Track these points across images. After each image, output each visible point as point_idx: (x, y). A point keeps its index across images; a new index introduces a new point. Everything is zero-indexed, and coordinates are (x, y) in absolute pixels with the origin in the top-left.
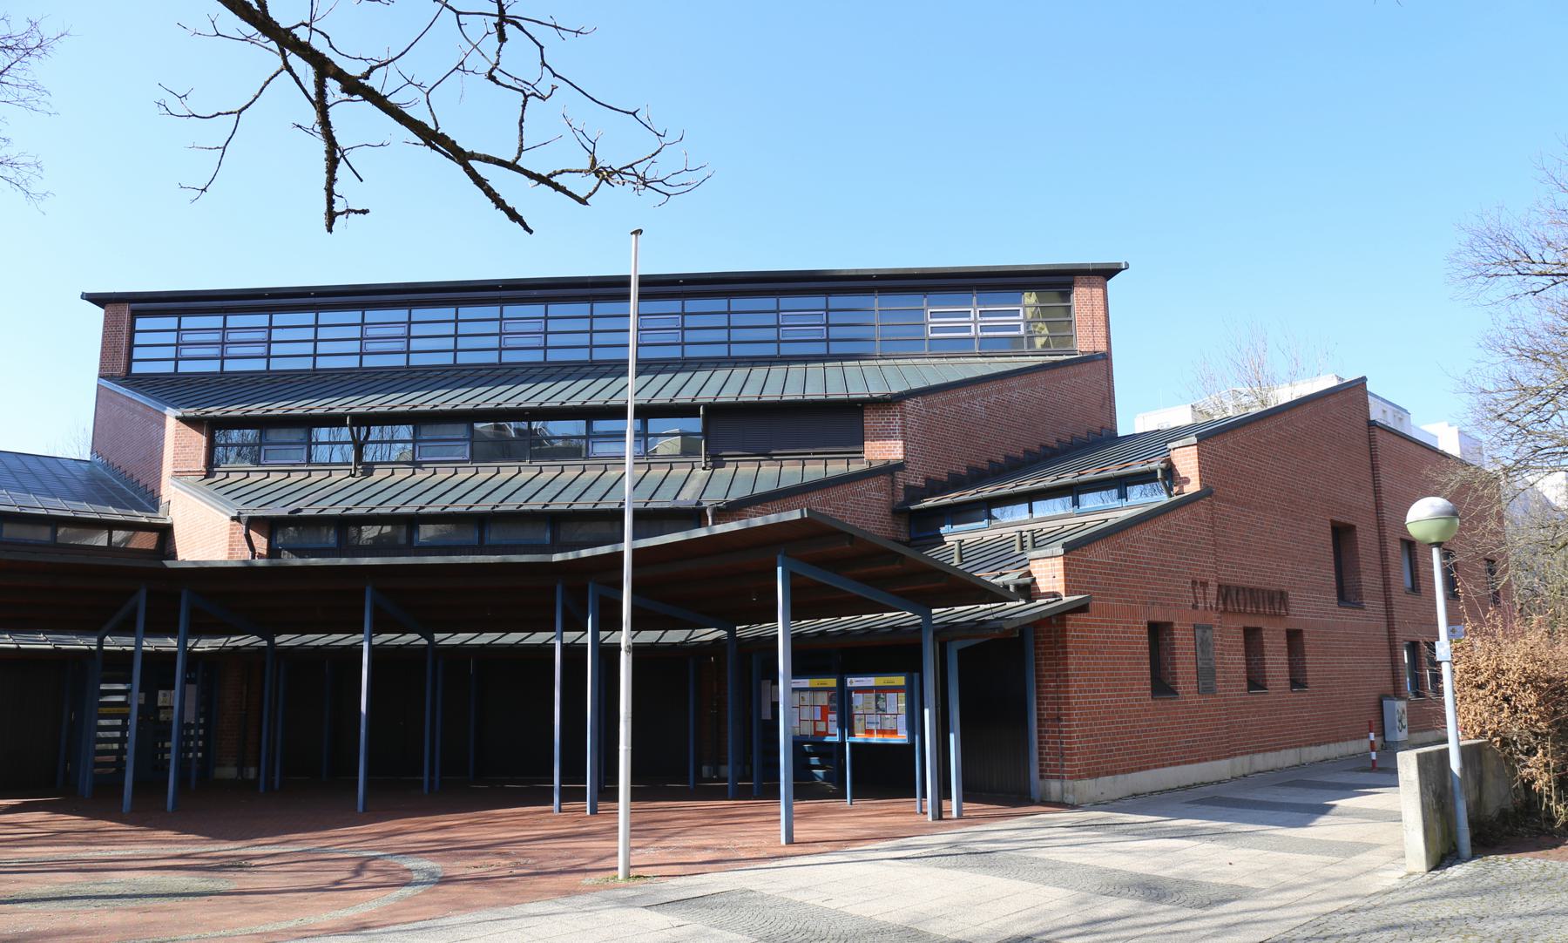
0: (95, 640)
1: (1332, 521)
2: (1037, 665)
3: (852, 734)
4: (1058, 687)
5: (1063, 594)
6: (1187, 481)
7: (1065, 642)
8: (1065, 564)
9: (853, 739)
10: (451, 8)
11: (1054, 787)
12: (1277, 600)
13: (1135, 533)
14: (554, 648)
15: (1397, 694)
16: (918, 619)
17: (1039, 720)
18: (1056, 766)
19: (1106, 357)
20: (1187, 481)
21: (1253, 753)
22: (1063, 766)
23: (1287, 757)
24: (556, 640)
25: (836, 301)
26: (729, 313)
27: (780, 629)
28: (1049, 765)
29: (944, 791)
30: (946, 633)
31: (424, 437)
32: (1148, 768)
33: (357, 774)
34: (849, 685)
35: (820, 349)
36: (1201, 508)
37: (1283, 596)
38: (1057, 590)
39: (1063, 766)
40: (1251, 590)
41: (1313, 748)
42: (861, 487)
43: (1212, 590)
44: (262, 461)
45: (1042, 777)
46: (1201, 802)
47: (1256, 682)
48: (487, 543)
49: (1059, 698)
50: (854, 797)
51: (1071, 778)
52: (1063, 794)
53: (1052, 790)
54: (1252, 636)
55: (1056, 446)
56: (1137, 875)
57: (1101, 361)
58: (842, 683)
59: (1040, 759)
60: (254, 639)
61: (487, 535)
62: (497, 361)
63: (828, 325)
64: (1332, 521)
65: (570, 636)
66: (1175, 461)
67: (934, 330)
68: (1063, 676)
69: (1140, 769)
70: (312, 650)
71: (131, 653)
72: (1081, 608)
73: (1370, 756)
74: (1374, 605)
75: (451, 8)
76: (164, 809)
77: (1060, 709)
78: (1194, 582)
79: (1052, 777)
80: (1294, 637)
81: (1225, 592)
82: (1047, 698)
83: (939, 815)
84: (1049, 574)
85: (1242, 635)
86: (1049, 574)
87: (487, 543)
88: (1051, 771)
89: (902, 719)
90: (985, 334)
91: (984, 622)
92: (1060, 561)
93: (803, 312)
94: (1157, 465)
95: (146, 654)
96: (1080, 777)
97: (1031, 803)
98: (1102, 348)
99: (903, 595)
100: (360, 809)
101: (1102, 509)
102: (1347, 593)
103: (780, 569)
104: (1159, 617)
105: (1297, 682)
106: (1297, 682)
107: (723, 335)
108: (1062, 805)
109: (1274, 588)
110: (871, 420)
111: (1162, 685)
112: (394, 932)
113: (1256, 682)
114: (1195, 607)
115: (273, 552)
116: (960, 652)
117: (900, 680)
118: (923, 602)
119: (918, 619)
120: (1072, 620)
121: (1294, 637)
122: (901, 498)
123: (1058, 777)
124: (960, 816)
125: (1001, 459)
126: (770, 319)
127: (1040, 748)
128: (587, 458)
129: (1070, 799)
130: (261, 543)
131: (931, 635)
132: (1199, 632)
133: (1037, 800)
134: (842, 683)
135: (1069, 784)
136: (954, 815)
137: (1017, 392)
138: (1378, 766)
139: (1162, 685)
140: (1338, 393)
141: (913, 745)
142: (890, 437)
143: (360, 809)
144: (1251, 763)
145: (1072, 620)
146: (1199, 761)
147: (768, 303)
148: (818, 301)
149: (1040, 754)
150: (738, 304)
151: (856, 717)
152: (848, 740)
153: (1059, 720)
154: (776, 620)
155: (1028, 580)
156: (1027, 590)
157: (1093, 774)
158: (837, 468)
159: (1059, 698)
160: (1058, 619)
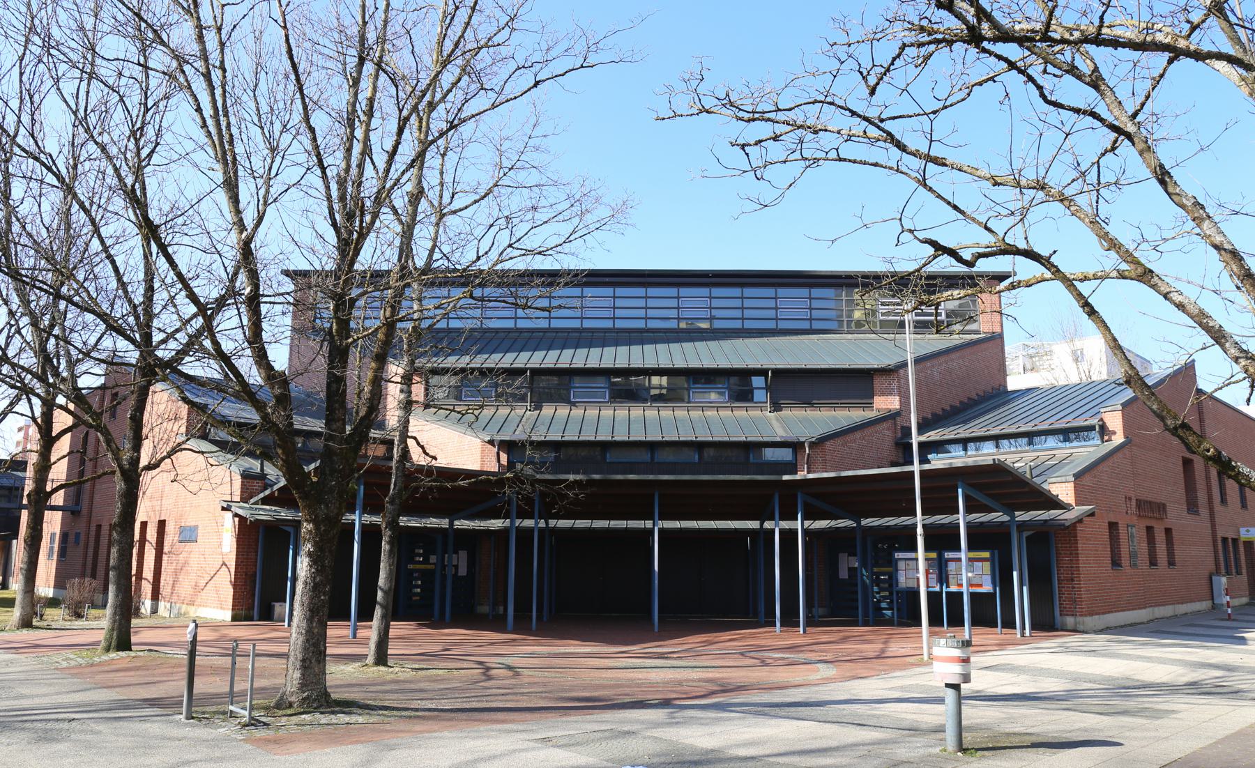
0: (447, 520)
1: (1183, 457)
2: (1056, 547)
3: (948, 586)
4: (1072, 560)
5: (1074, 505)
6: (1114, 433)
7: (1076, 533)
8: (1075, 487)
9: (949, 590)
10: (902, 225)
11: (1070, 621)
12: (1161, 508)
13: (1100, 467)
14: (959, 527)
15: (1218, 573)
16: (1006, 518)
17: (1058, 580)
18: (1070, 608)
19: (1001, 336)
20: (1114, 433)
21: (1154, 606)
22: (1076, 608)
23: (1167, 611)
24: (776, 526)
25: (816, 292)
26: (742, 298)
27: (961, 519)
28: (1065, 608)
30: (1022, 526)
31: (577, 385)
32: (1112, 612)
34: (946, 557)
35: (806, 325)
36: (1126, 451)
37: (1164, 505)
38: (1069, 502)
39: (1076, 608)
40: (1150, 502)
41: (1180, 605)
42: (880, 427)
43: (1134, 503)
44: (464, 399)
45: (1061, 615)
47: (1153, 562)
48: (656, 461)
49: (1072, 567)
50: (949, 625)
51: (1081, 615)
52: (1076, 625)
53: (1068, 623)
54: (1149, 529)
55: (976, 398)
56: (824, 756)
57: (996, 339)
58: (940, 556)
59: (1060, 604)
60: (850, 522)
61: (656, 456)
62: (579, 326)
63: (811, 309)
64: (1183, 457)
65: (786, 525)
66: (1106, 420)
67: (883, 314)
68: (1074, 554)
69: (1109, 612)
70: (978, 526)
73: (1227, 611)
74: (1204, 512)
75: (902, 225)
76: (531, 630)
77: (1072, 574)
78: (1126, 498)
79: (1067, 615)
80: (1168, 531)
81: (1140, 503)
82: (1063, 567)
83: (1023, 635)
84: (1064, 491)
85: (1164, 533)
87: (656, 461)
88: (1067, 611)
89: (989, 578)
90: (918, 318)
92: (1072, 484)
93: (793, 301)
94: (1094, 421)
96: (1086, 615)
97: (1057, 630)
98: (998, 330)
99: (1003, 504)
100: (656, 629)
102: (1192, 507)
103: (960, 491)
105: (1171, 563)
106: (1171, 563)
107: (738, 313)
108: (1075, 631)
109: (1159, 501)
110: (878, 382)
111: (1116, 563)
113: (1153, 562)
114: (1127, 513)
115: (511, 465)
117: (986, 554)
118: (1011, 508)
119: (1006, 518)
121: (1168, 531)
122: (899, 435)
123: (1073, 615)
124: (1031, 636)
125: (948, 408)
126: (772, 303)
127: (1060, 597)
128: (689, 402)
129: (1081, 628)
130: (504, 458)
131: (1015, 528)
132: (1129, 528)
133: (1060, 628)
134: (940, 556)
135: (1079, 619)
137: (956, 362)
138: (1233, 617)
139: (1116, 563)
140: (173, 51)
141: (996, 592)
142: (891, 394)
143: (656, 629)
144: (1153, 613)
146: (1133, 609)
147: (770, 292)
148: (804, 292)
149: (1060, 601)
150: (748, 292)
151: (950, 576)
152: (944, 589)
153: (1073, 580)
157: (1091, 614)
158: (857, 415)
159: (1072, 567)
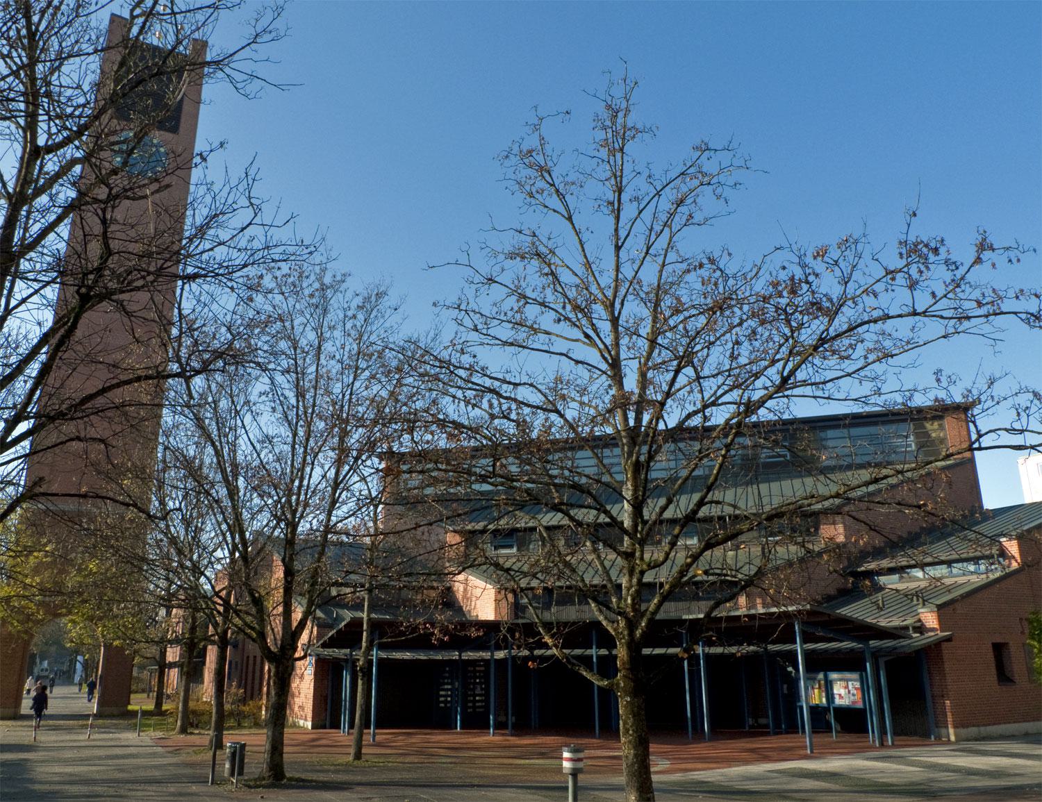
29: (883, 732)
30: (876, 654)
33: (599, 701)
46: (862, 770)
71: (488, 660)
72: (948, 639)
78: (1021, 619)
83: (882, 745)
84: (930, 619)
86: (930, 619)
91: (896, 648)
95: (496, 660)
101: (969, 576)
104: (999, 640)
111: (1004, 676)
112: (600, 339)
116: (886, 662)
120: (945, 645)
136: (890, 743)
139: (1004, 676)
145: (945, 645)
154: (796, 643)
155: (919, 624)
156: (920, 628)
160: (938, 644)
